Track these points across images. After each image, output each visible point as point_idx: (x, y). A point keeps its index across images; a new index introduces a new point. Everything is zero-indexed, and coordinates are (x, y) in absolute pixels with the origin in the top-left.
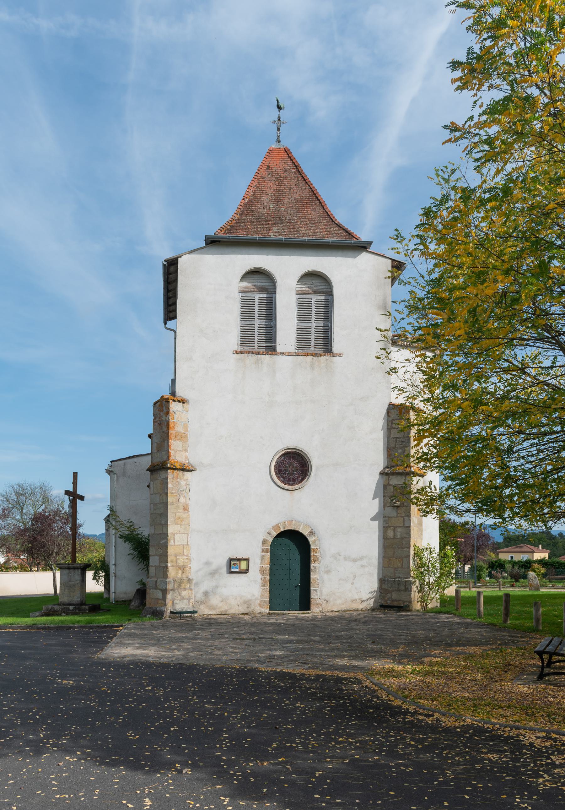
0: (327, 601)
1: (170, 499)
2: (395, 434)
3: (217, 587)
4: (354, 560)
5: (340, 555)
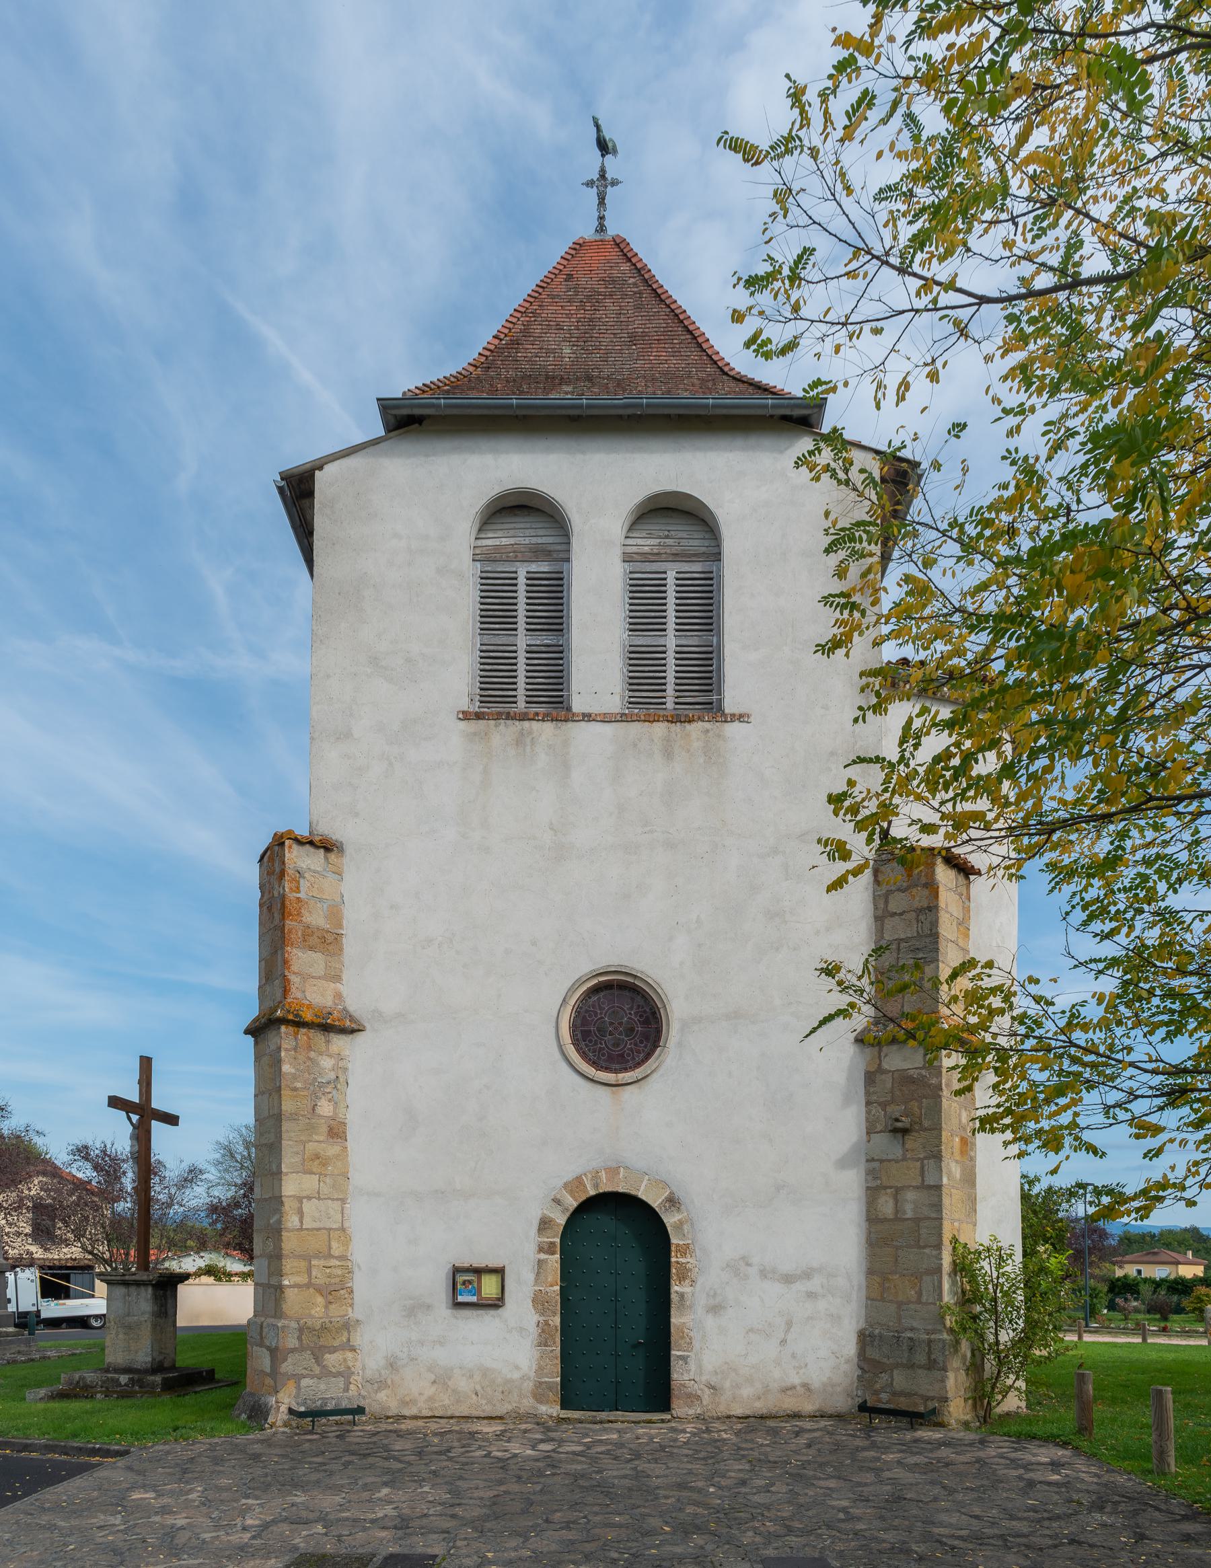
0: (713, 1388)
2: (897, 929)
4: (788, 1279)
5: (748, 1264)
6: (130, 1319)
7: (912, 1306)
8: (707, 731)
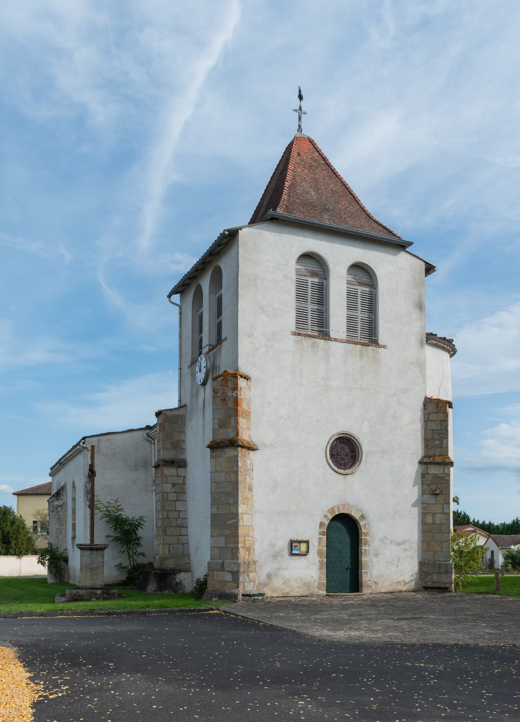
0: (376, 583)
1: (240, 478)
2: (432, 426)
3: (279, 569)
4: (399, 544)
5: (387, 539)
6: (93, 565)
7: (439, 553)
8: (374, 350)
